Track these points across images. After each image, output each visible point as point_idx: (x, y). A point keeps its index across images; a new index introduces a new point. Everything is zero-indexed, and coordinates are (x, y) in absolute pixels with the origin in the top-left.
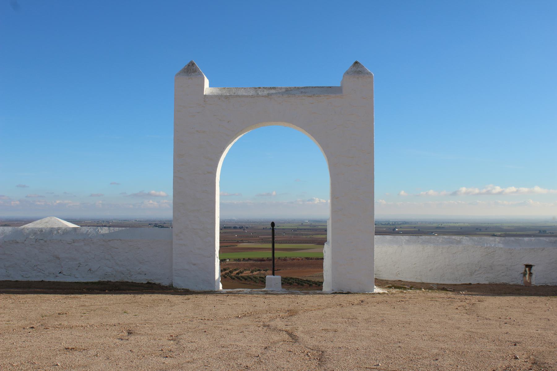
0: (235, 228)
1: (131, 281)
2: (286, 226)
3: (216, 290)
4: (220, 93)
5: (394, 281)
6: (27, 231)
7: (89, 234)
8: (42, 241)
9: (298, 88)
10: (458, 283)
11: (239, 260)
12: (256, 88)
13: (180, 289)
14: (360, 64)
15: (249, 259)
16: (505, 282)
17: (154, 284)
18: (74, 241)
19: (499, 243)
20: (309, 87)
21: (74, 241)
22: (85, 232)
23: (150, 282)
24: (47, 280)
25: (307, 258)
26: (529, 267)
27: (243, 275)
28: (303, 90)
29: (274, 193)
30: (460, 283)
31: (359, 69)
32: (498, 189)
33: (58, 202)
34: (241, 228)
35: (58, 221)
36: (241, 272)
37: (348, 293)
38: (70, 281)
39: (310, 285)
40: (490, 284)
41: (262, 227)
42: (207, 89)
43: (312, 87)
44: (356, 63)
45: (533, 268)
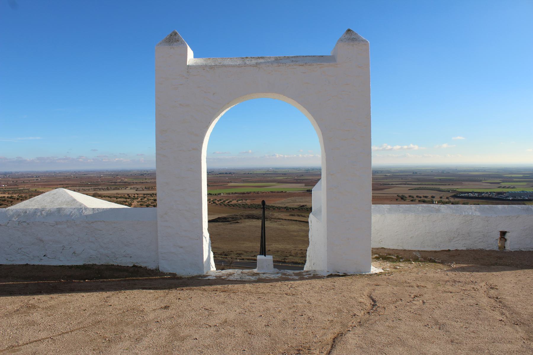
0: (226, 173)
1: (116, 264)
2: (258, 172)
3: (205, 274)
4: (204, 63)
5: (378, 249)
6: (11, 213)
7: (72, 216)
8: (25, 224)
9: (288, 57)
10: (438, 249)
11: (229, 194)
12: (243, 58)
13: (166, 274)
14: (353, 32)
15: (236, 193)
16: (481, 248)
17: (141, 267)
18: (57, 223)
19: (475, 210)
20: (300, 56)
21: (57, 223)
22: (68, 213)
23: (136, 265)
24: (32, 263)
25: (272, 192)
26: (503, 234)
27: (232, 203)
28: (294, 59)
29: (250, 151)
30: (440, 250)
31: (353, 37)
32: (389, 147)
33: (117, 159)
34: (230, 173)
35: (65, 192)
36: (231, 202)
37: (345, 275)
38: (55, 265)
39: (274, 209)
40: (468, 250)
41: (243, 173)
42: (191, 57)
43: (303, 56)
44: (349, 30)
45: (507, 234)
